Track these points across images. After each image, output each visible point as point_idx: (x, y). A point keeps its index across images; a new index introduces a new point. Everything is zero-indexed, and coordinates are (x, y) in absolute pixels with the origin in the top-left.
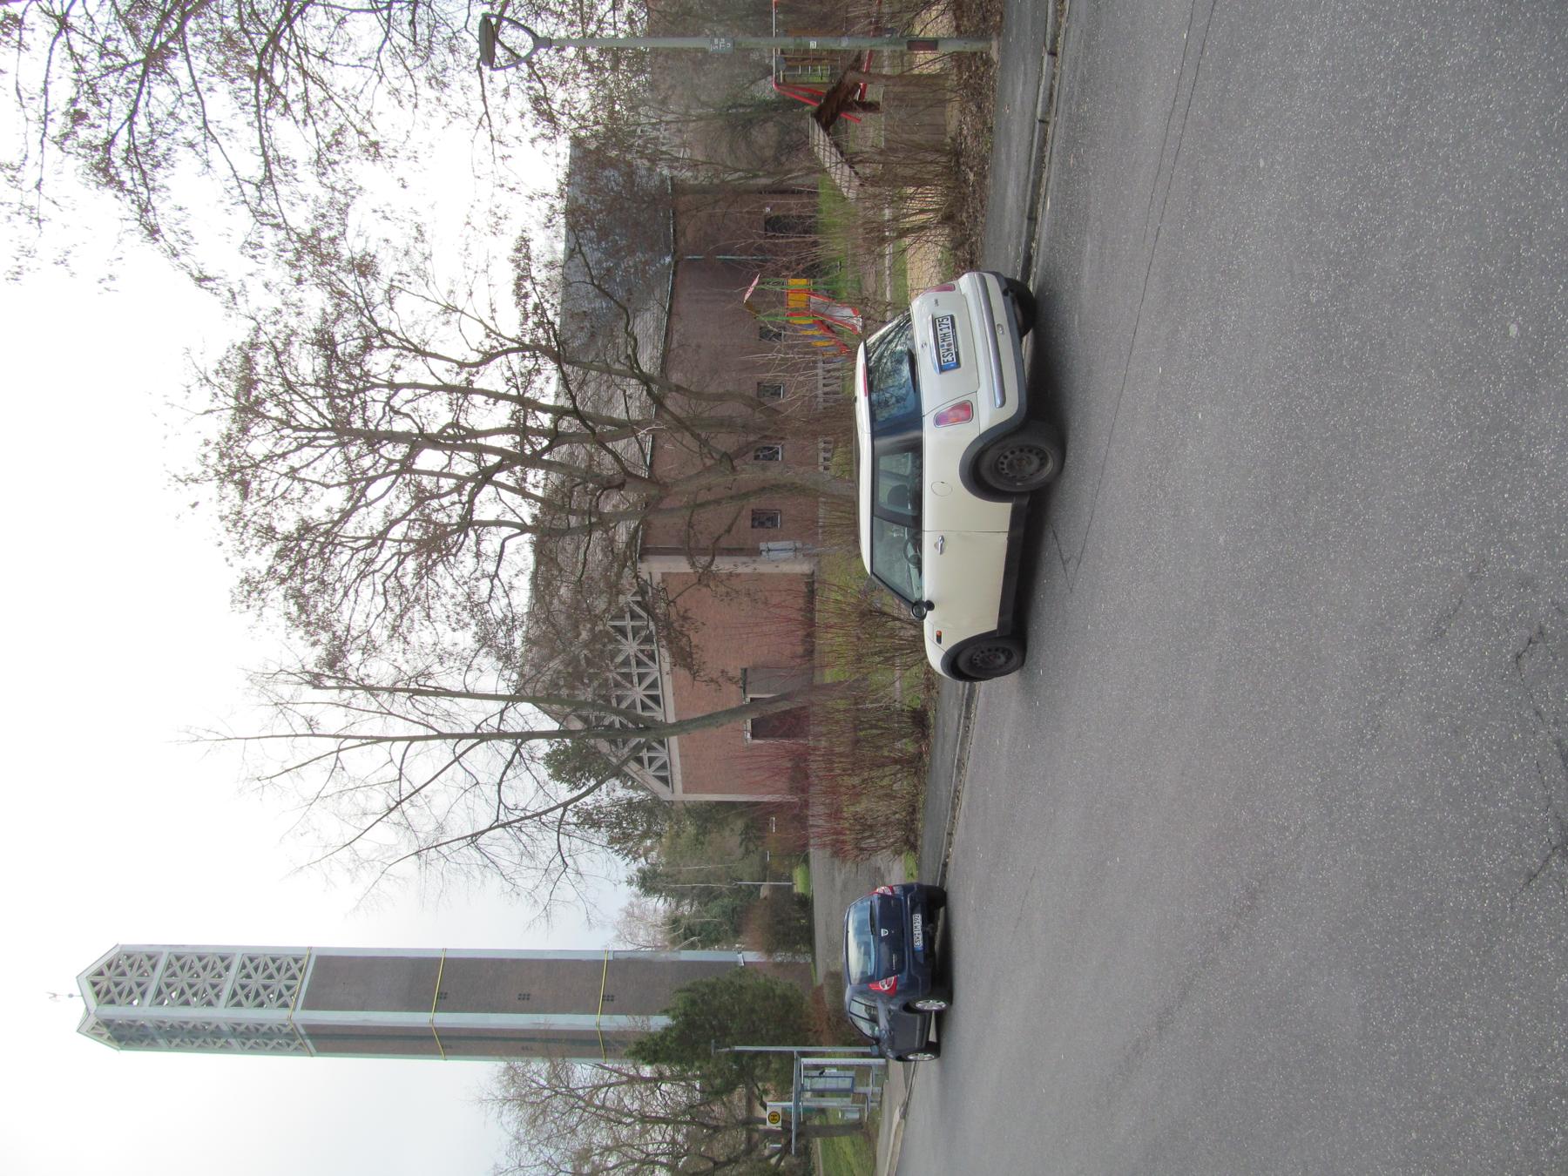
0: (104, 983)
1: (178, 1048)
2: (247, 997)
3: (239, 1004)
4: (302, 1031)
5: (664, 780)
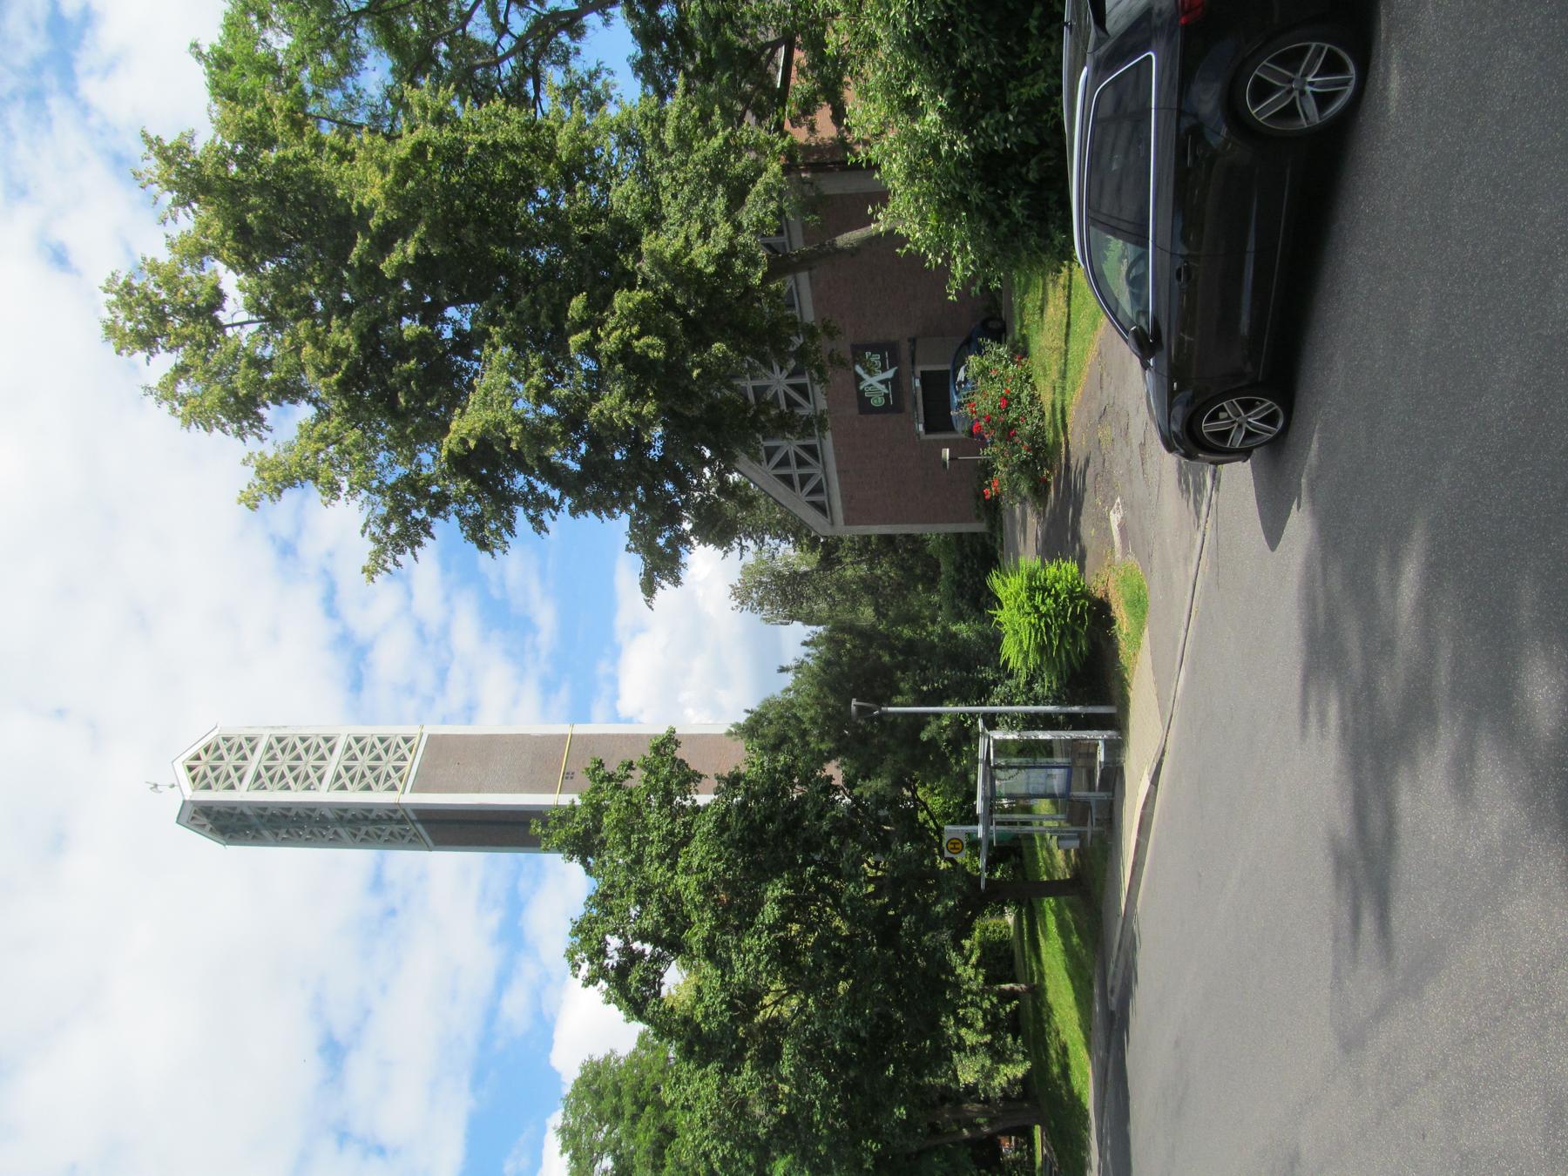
0: (202, 768)
1: (284, 842)
2: (352, 780)
3: (343, 787)
4: (414, 817)
5: (821, 508)
